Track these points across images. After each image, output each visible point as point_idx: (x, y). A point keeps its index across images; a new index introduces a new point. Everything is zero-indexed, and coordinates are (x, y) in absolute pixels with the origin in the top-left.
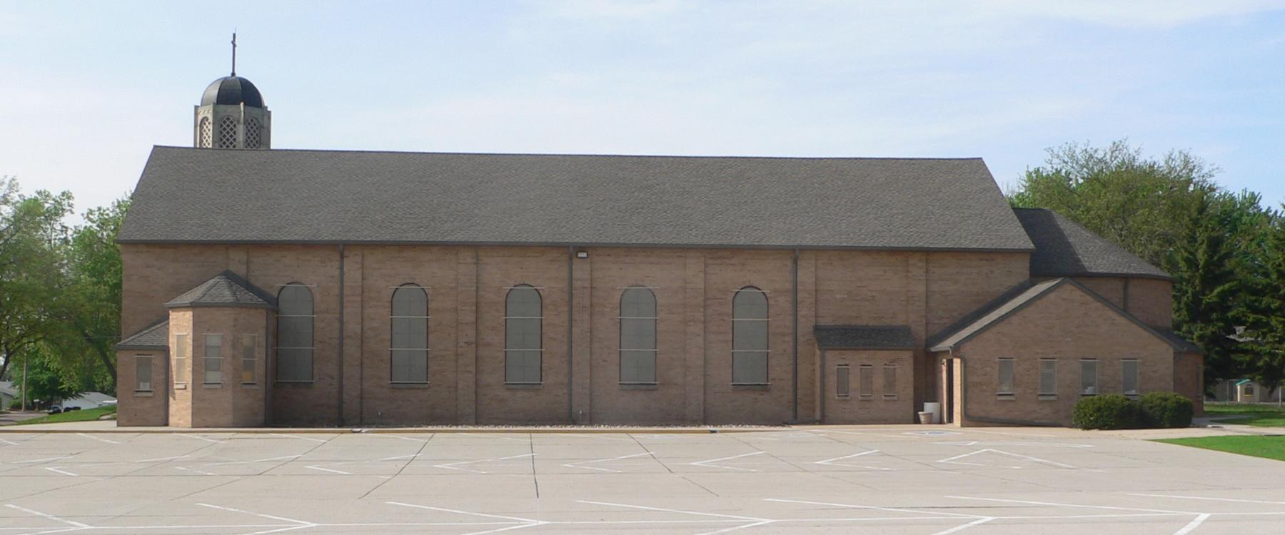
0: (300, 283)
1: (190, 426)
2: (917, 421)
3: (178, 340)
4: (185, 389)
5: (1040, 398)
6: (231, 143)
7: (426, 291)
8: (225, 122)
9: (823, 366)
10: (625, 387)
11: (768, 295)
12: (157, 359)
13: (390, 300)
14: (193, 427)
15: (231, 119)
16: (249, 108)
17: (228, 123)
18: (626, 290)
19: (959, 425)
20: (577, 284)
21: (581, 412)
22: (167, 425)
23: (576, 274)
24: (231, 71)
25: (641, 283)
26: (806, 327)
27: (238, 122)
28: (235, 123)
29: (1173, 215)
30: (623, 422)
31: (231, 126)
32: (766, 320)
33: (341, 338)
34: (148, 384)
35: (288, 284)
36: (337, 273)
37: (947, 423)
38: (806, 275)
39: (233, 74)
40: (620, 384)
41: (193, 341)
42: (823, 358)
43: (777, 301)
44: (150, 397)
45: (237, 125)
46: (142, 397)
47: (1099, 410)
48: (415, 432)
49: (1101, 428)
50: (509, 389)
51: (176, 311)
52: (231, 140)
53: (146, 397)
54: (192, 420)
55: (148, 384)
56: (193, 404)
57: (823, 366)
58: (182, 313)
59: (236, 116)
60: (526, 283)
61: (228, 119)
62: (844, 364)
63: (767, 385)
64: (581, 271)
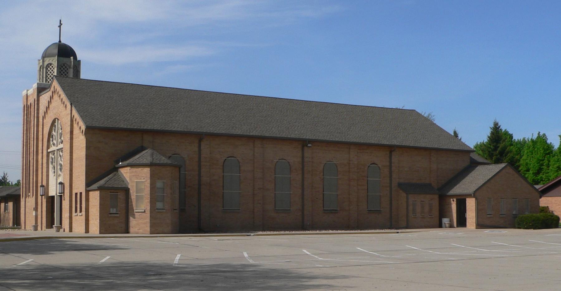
0: (179, 154)
1: (149, 233)
2: (440, 226)
3: (136, 184)
4: (145, 212)
5: (501, 216)
7: (239, 161)
8: (62, 67)
9: (407, 202)
11: (380, 168)
12: (121, 196)
13: (222, 165)
14: (151, 234)
15: (66, 65)
16: (61, 58)
17: (64, 67)
18: (326, 163)
19: (474, 227)
20: (306, 160)
21: (308, 224)
22: (128, 233)
23: (306, 155)
24: (59, 40)
25: (331, 160)
27: (70, 67)
29: (176, 118)
32: (276, 176)
33: (200, 185)
35: (228, 158)
36: (196, 149)
37: (458, 226)
38: (395, 158)
39: (60, 41)
40: (324, 210)
41: (151, 185)
42: (407, 199)
43: (383, 171)
44: (117, 217)
46: (113, 217)
47: (534, 221)
48: (200, 236)
49: (535, 229)
51: (137, 168)
53: (115, 217)
54: (150, 230)
55: (115, 209)
56: (150, 221)
57: (407, 202)
58: (140, 169)
59: (68, 63)
60: (284, 158)
61: (64, 65)
62: (415, 200)
63: (380, 210)
64: (308, 153)
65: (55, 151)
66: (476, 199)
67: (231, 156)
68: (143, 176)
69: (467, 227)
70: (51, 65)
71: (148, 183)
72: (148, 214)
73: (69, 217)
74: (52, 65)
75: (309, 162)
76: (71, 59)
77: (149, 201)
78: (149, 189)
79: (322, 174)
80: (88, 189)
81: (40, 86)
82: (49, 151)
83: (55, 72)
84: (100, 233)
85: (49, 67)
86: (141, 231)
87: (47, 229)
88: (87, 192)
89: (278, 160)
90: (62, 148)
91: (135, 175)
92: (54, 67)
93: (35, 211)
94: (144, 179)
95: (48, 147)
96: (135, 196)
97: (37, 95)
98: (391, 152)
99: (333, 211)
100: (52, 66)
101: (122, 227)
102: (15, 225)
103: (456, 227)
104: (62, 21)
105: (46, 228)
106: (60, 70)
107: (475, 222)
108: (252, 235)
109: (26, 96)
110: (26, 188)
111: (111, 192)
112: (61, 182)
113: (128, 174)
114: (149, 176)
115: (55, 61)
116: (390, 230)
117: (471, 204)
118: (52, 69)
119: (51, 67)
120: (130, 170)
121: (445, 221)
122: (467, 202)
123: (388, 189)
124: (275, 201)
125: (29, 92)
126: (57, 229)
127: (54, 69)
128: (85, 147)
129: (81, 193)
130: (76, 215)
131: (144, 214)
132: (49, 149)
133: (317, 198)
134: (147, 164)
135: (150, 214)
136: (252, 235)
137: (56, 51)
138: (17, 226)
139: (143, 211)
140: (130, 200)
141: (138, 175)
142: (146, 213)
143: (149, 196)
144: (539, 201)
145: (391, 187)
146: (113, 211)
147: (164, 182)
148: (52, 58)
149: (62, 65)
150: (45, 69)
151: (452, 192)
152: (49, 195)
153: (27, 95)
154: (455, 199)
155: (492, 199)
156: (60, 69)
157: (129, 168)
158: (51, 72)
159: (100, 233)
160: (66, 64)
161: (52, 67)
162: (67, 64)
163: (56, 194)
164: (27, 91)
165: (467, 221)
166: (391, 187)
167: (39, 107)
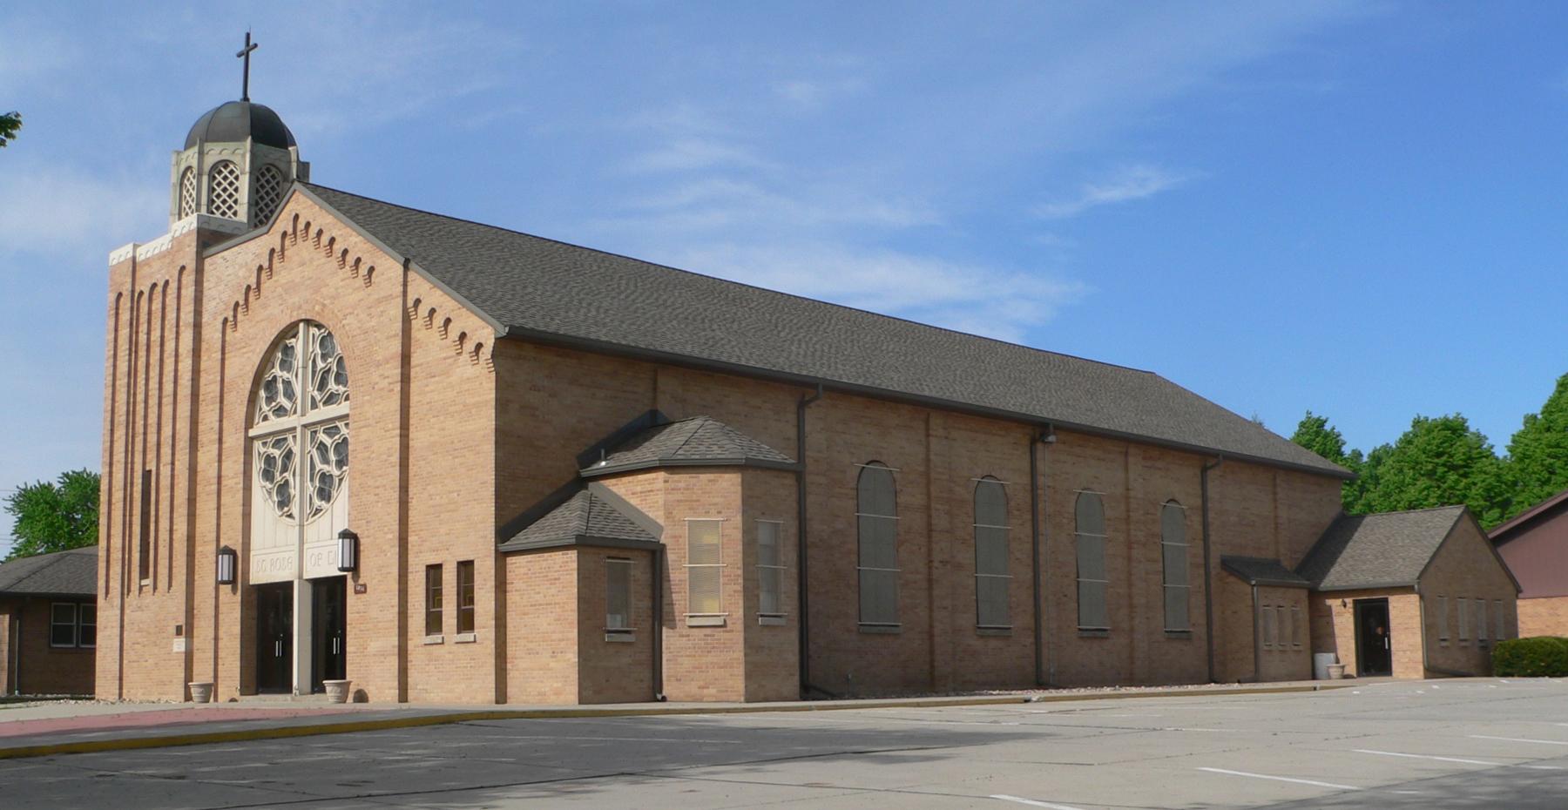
1: (742, 699)
6: (230, 208)
7: (895, 475)
10: (1085, 634)
14: (747, 701)
15: (274, 171)
16: (263, 147)
20: (1041, 480)
22: (1314, 677)
26: (1215, 561)
28: (237, 172)
30: (1180, 682)
31: (231, 178)
34: (619, 617)
40: (1080, 629)
41: (745, 532)
44: (630, 644)
45: (240, 177)
48: (918, 705)
49: (1552, 675)
50: (982, 637)
52: (230, 202)
53: (623, 643)
54: (746, 687)
59: (282, 166)
61: (268, 170)
65: (295, 428)
66: (1421, 598)
67: (875, 458)
68: (715, 504)
69: (1394, 674)
70: (226, 167)
71: (736, 528)
72: (737, 636)
73: (396, 650)
74: (232, 166)
75: (1049, 487)
76: (289, 153)
77: (739, 588)
78: (740, 548)
79: (1073, 524)
80: (507, 546)
81: (205, 226)
82: (252, 433)
83: (240, 189)
84: (580, 703)
85: (220, 172)
86: (712, 691)
87: (244, 697)
88: (501, 557)
89: (979, 480)
90: (347, 416)
91: (687, 501)
92: (237, 172)
93: (186, 637)
94: (720, 512)
95: (249, 423)
96: (687, 570)
97: (197, 252)
98: (1204, 470)
99: (1099, 634)
100: (229, 169)
101: (642, 681)
102: (16, 692)
103: (1355, 676)
104: (251, 36)
105: (241, 694)
106: (258, 185)
107: (1421, 660)
108: (1034, 699)
109: (131, 263)
110: (126, 562)
111: (609, 558)
112: (346, 530)
113: (660, 498)
114: (739, 502)
115: (243, 156)
116: (1041, 691)
117: (1405, 615)
118: (231, 178)
119: (226, 172)
120: (666, 481)
121: (1324, 660)
122: (1390, 607)
123: (1202, 571)
124: (977, 600)
125: (139, 251)
126: (341, 692)
127: (237, 178)
128: (494, 403)
129: (466, 567)
130: (472, 639)
131: (719, 633)
132: (252, 427)
133: (1065, 596)
134: (734, 462)
135: (745, 631)
136: (1034, 699)
137: (246, 122)
138: (20, 693)
139: (721, 623)
140: (665, 585)
141: (698, 501)
142: (728, 628)
143: (740, 572)
144: (1515, 607)
145: (1207, 565)
146: (615, 622)
147: (777, 525)
148: (232, 145)
149: (264, 170)
150: (205, 179)
151: (1332, 580)
152: (251, 583)
153: (134, 258)
154: (1349, 601)
155: (1446, 598)
156: (258, 180)
157: (662, 475)
158: (225, 190)
159: (580, 703)
160: (275, 166)
161: (231, 172)
162: (277, 168)
163: (300, 577)
164: (135, 247)
165: (1394, 658)
166: (1207, 565)
167: (202, 292)
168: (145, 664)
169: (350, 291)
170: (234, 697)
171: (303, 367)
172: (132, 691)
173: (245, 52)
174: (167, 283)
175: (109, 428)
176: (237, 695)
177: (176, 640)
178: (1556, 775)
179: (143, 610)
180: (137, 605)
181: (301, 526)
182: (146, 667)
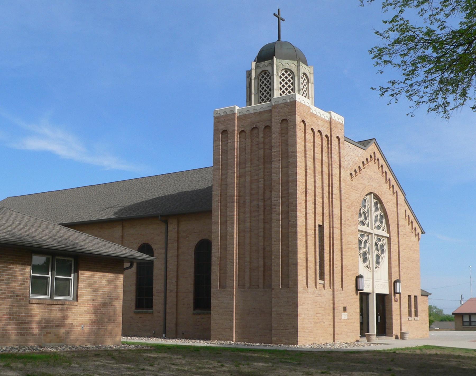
85: (289, 75)
168: (323, 324)
169: (388, 194)
170: (357, 339)
171: (372, 211)
172: (317, 338)
173: (279, 16)
174: (374, 153)
175: (399, 215)
176: (359, 338)
177: (343, 313)
178: (150, 351)
179: (321, 297)
180: (318, 293)
181: (373, 272)
182: (324, 326)
